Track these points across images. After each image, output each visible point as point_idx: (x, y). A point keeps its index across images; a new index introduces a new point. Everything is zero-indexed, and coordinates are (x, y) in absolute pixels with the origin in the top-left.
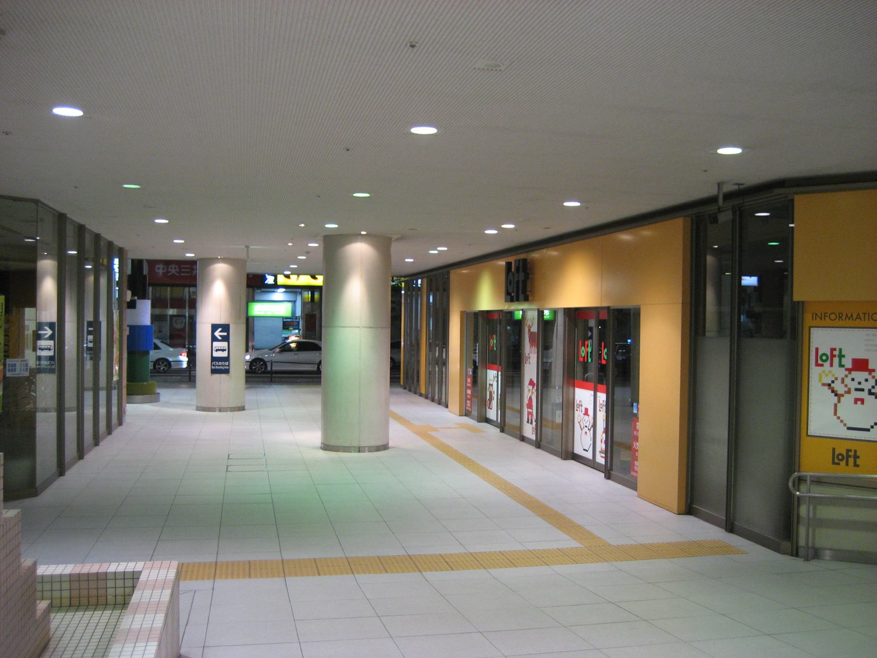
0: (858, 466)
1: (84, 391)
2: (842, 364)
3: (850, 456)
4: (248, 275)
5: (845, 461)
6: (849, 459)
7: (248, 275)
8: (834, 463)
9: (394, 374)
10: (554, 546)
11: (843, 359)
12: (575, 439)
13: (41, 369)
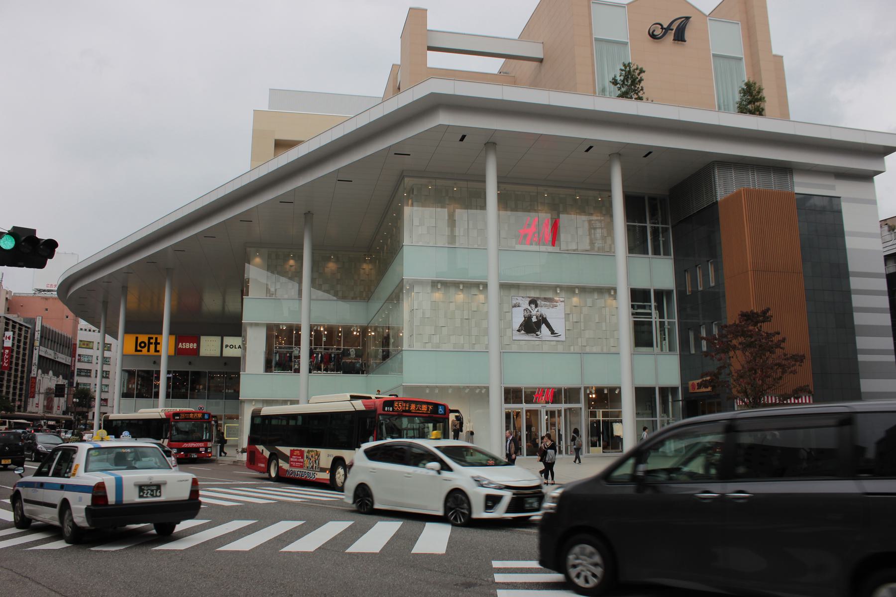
0: (158, 351)
1: (559, 214)
2: (158, 349)
3: (152, 343)
4: (631, 289)
5: (147, 347)
6: (151, 345)
7: (631, 289)
8: (136, 350)
9: (639, 307)
10: (301, 523)
11: (158, 346)
12: (752, 416)
13: (375, 411)
